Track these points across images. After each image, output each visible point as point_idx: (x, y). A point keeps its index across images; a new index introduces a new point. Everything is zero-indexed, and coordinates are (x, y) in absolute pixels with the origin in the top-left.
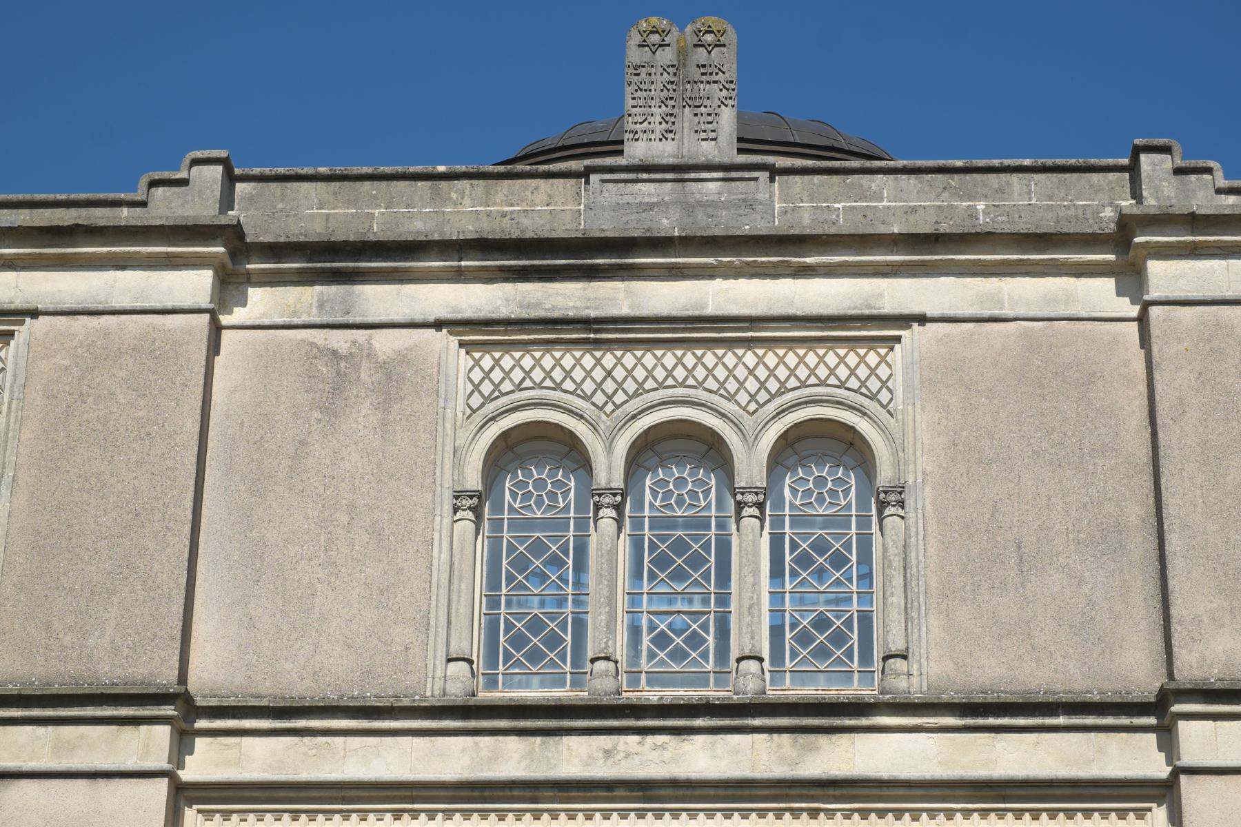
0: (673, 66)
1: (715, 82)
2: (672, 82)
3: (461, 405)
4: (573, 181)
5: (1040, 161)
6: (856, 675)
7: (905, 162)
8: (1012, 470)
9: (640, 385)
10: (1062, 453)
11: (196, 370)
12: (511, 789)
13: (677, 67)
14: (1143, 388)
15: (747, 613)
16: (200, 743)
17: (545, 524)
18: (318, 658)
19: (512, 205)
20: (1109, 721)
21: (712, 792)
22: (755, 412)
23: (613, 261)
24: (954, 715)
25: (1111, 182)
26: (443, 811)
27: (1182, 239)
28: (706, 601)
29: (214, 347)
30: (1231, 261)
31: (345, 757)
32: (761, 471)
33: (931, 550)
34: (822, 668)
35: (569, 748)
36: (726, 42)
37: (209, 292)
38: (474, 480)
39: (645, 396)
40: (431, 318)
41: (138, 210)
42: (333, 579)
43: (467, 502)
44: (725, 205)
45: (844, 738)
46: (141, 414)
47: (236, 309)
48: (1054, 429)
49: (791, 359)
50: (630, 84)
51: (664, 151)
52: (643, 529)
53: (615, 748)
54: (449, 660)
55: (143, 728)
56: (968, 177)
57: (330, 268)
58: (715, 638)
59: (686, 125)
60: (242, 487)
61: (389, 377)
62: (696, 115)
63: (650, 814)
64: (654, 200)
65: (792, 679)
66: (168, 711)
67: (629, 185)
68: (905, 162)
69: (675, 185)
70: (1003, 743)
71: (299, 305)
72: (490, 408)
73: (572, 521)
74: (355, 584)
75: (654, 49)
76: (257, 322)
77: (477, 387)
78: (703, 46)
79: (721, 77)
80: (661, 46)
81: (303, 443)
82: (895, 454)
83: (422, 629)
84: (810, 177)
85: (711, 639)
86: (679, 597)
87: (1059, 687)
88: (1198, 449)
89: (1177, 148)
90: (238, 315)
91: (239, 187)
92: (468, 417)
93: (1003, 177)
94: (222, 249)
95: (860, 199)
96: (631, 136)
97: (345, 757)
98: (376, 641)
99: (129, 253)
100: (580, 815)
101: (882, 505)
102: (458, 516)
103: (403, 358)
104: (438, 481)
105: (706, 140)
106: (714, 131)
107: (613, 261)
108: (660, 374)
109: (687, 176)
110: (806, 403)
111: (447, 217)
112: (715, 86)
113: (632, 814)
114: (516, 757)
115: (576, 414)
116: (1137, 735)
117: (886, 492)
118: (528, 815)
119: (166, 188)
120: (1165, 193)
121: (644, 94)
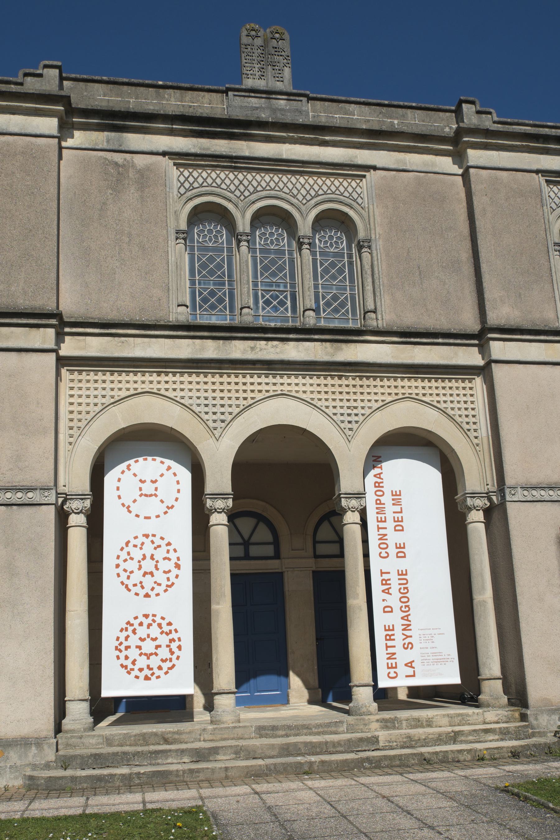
0: (262, 46)
1: (281, 56)
2: (262, 54)
3: (176, 192)
4: (220, 95)
5: (419, 105)
6: (351, 321)
7: (364, 100)
8: (415, 235)
9: (255, 188)
10: (434, 229)
11: (54, 164)
12: (210, 363)
13: (264, 46)
14: (464, 204)
15: (307, 290)
16: (67, 338)
17: (214, 249)
18: (119, 302)
19: (193, 103)
20: (459, 341)
21: (298, 367)
22: (306, 203)
23: (242, 131)
24: (397, 337)
25: (447, 117)
26: (179, 372)
27: (483, 140)
28: (285, 287)
29: (60, 157)
30: (501, 153)
31: (134, 347)
32: (309, 230)
33: (384, 267)
34: (336, 317)
35: (235, 346)
36: (285, 38)
37: (57, 129)
38: (183, 226)
39: (257, 193)
40: (161, 151)
41: (19, 87)
42: (123, 267)
43: (182, 236)
44: (289, 111)
45: (353, 345)
46: (28, 183)
47: (68, 140)
48: (430, 219)
49: (320, 182)
50: (244, 52)
51: (261, 84)
52: (256, 254)
53: (255, 346)
54: (179, 306)
55: (42, 329)
56: (390, 109)
57: (112, 124)
58: (291, 302)
59: (270, 73)
60: (77, 222)
61: (142, 176)
62: (274, 69)
63: (271, 376)
64: (258, 106)
65: (324, 321)
66: (54, 322)
67: (246, 98)
68: (364, 100)
69: (266, 100)
70: (417, 349)
71: (97, 141)
72: (189, 194)
73: (225, 248)
74: (133, 269)
75: (253, 38)
76: (79, 146)
77: (182, 184)
78: (275, 39)
79: (283, 53)
80: (256, 37)
81: (104, 204)
82: (365, 226)
83: (166, 291)
84: (324, 102)
85: (289, 303)
86: (274, 284)
87: (438, 327)
88: (492, 230)
89: (477, 102)
90: (70, 142)
91: (65, 83)
92: (179, 198)
93: (404, 110)
94: (62, 108)
95: (345, 114)
96: (246, 76)
97: (134, 347)
98: (145, 296)
99: (17, 106)
100: (240, 375)
101: (360, 248)
102: (178, 242)
103: (148, 168)
104: (169, 225)
105: (278, 81)
106: (282, 77)
107: (242, 131)
108: (264, 184)
109: (271, 96)
110: (327, 201)
111: (164, 105)
112: (281, 58)
113: (263, 376)
114: (212, 349)
115: (228, 199)
116: (470, 348)
117: (363, 242)
118: (218, 375)
119: (32, 78)
120: (473, 121)
121: (250, 58)
